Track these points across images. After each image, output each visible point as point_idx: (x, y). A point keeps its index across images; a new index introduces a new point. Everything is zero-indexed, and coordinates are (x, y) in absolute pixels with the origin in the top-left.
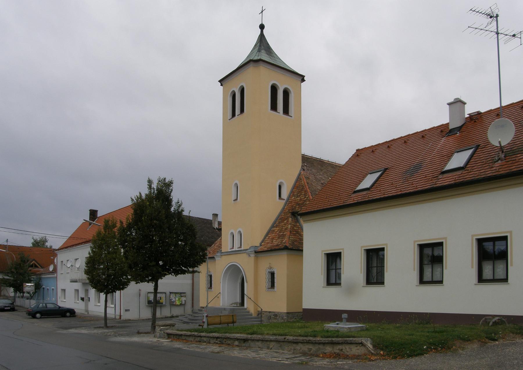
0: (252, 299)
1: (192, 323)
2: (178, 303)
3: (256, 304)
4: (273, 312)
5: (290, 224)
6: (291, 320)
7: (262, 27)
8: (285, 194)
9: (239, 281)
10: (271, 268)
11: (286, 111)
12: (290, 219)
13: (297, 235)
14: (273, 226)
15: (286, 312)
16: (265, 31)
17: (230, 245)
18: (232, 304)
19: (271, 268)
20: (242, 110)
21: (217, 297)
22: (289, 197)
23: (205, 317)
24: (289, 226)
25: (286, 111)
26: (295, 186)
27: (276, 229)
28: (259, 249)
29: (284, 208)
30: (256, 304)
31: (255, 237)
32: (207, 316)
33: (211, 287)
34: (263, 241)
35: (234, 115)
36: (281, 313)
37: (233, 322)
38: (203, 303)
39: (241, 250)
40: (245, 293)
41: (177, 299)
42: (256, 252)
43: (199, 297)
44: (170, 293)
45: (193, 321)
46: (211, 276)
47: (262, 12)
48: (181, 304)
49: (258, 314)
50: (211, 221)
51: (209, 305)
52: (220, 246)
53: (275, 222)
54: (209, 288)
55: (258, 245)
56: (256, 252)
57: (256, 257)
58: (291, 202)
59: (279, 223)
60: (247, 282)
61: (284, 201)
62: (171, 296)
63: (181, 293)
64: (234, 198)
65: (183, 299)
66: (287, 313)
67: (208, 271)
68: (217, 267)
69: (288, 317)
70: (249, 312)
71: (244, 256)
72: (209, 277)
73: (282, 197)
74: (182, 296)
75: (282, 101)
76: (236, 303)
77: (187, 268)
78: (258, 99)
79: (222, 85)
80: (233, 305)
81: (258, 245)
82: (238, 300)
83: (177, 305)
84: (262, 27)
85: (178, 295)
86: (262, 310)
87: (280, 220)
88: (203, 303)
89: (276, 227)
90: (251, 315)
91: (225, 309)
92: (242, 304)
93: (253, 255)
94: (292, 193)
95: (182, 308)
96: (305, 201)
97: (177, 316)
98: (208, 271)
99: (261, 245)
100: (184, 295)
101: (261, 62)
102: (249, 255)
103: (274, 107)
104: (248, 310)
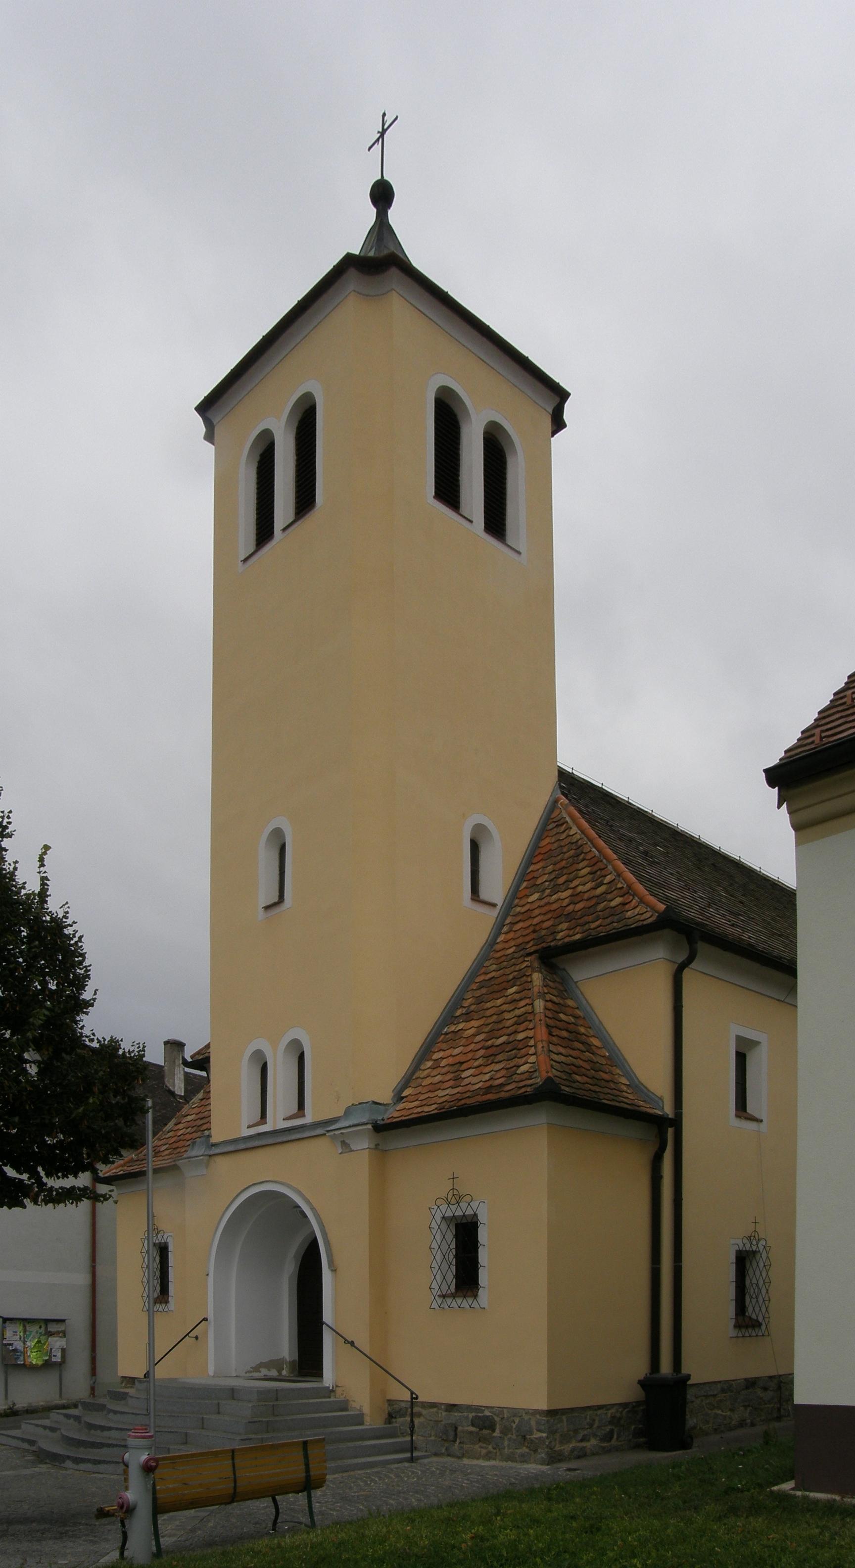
0: (363, 1342)
1: (77, 1461)
2: (34, 1358)
3: (380, 1367)
4: (469, 1408)
5: (542, 995)
6: (567, 1448)
7: (382, 195)
8: (496, 886)
9: (290, 1269)
10: (459, 1199)
11: (496, 522)
12: (537, 978)
13: (576, 1045)
14: (449, 1017)
15: (543, 1406)
16: (394, 215)
17: (248, 1110)
18: (257, 1369)
19: (459, 1199)
20: (305, 499)
21: (193, 1335)
22: (515, 895)
23: (135, 1474)
24: (539, 1005)
25: (496, 522)
26: (535, 853)
27: (470, 1028)
28: (394, 1113)
29: (491, 943)
30: (380, 1367)
31: (373, 1065)
32: (148, 1469)
33: (164, 1294)
34: (406, 1082)
35: (264, 531)
36: (515, 1412)
37: (308, 1485)
38: (129, 1361)
39: (302, 1127)
40: (327, 1316)
41: (31, 1343)
42: (379, 1128)
43: (114, 1334)
44: (5, 1320)
45: (81, 1453)
46: (163, 1250)
47: (382, 134)
48: (48, 1365)
49: (391, 1417)
50: (162, 1067)
51: (161, 1372)
52: (203, 1122)
53: (457, 1001)
54: (157, 1301)
55: (386, 1096)
56: (379, 1128)
57: (380, 1152)
58: (527, 915)
59: (479, 1001)
60: (334, 1270)
61: (494, 913)
62: (8, 1334)
63: (47, 1321)
64: (266, 893)
65: (57, 1343)
66: (551, 1413)
67: (152, 1228)
68: (197, 1210)
69: (552, 1432)
70: (344, 1406)
71: (321, 1149)
72: (155, 1253)
73: (485, 893)
74: (50, 1334)
75: (486, 444)
76: (276, 1364)
77: (34, 1174)
78: (377, 457)
79: (210, 437)
80: (264, 1372)
81: (386, 1096)
82: (285, 1347)
83: (33, 1368)
84: (382, 195)
85: (33, 1329)
86: (414, 1397)
87: (482, 988)
88: (129, 1361)
89: (468, 1016)
90: (359, 1419)
91: (233, 1393)
92: (309, 1360)
93: (363, 1144)
94: (525, 879)
95: (52, 1377)
96: (601, 898)
97: (31, 1412)
98: (152, 1228)
99: (399, 1098)
100: (61, 1327)
101: (394, 272)
102: (344, 1144)
103: (448, 490)
104: (339, 1396)
